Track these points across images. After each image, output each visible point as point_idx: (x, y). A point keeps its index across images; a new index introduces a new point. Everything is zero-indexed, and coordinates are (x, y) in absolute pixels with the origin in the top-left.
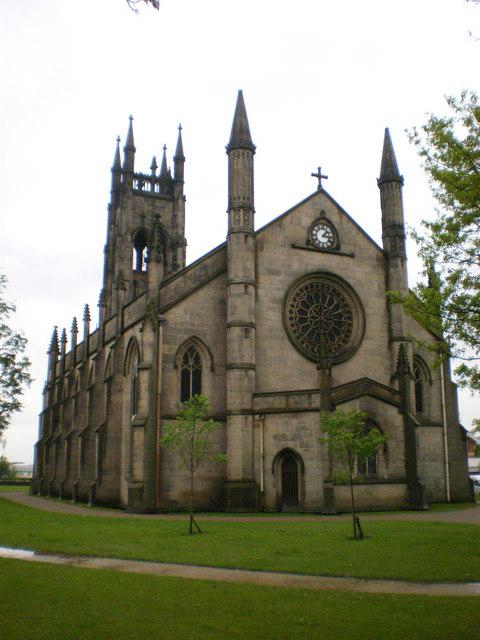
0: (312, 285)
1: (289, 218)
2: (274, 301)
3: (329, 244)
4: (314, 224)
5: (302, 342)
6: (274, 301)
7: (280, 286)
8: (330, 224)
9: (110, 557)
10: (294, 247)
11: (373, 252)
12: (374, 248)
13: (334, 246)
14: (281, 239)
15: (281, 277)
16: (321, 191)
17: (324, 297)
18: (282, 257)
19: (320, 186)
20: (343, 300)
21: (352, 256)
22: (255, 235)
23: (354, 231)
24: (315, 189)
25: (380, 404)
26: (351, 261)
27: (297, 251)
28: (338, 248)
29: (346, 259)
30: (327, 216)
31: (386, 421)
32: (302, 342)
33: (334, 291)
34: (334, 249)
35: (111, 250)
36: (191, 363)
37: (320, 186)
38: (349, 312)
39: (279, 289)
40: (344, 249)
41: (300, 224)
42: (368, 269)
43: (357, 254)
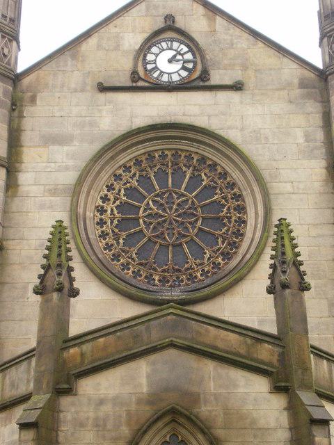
0: (150, 156)
1: (93, 41)
2: (53, 192)
4: (153, 39)
5: (125, 267)
6: (53, 192)
7: (71, 163)
8: (185, 36)
10: (103, 89)
11: (291, 71)
12: (246, 35)
14: (75, 78)
15: (75, 147)
17: (177, 172)
18: (75, 110)
20: (224, 175)
21: (237, 87)
22: (16, 79)
23: (244, 41)
25: (210, 368)
26: (234, 96)
27: (110, 95)
28: (205, 75)
29: (222, 96)
30: (180, 23)
31: (227, 411)
32: (125, 267)
33: (203, 159)
34: (197, 81)
38: (238, 197)
39: (67, 168)
41: (117, 48)
42: (278, 106)
43: (250, 82)
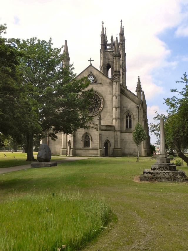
3: (93, 81)
9: (88, 157)
13: (95, 81)
16: (91, 65)
19: (91, 64)
21: (101, 84)
24: (90, 65)
28: (96, 82)
35: (125, 70)
36: (129, 117)
37: (91, 64)
40: (99, 82)
